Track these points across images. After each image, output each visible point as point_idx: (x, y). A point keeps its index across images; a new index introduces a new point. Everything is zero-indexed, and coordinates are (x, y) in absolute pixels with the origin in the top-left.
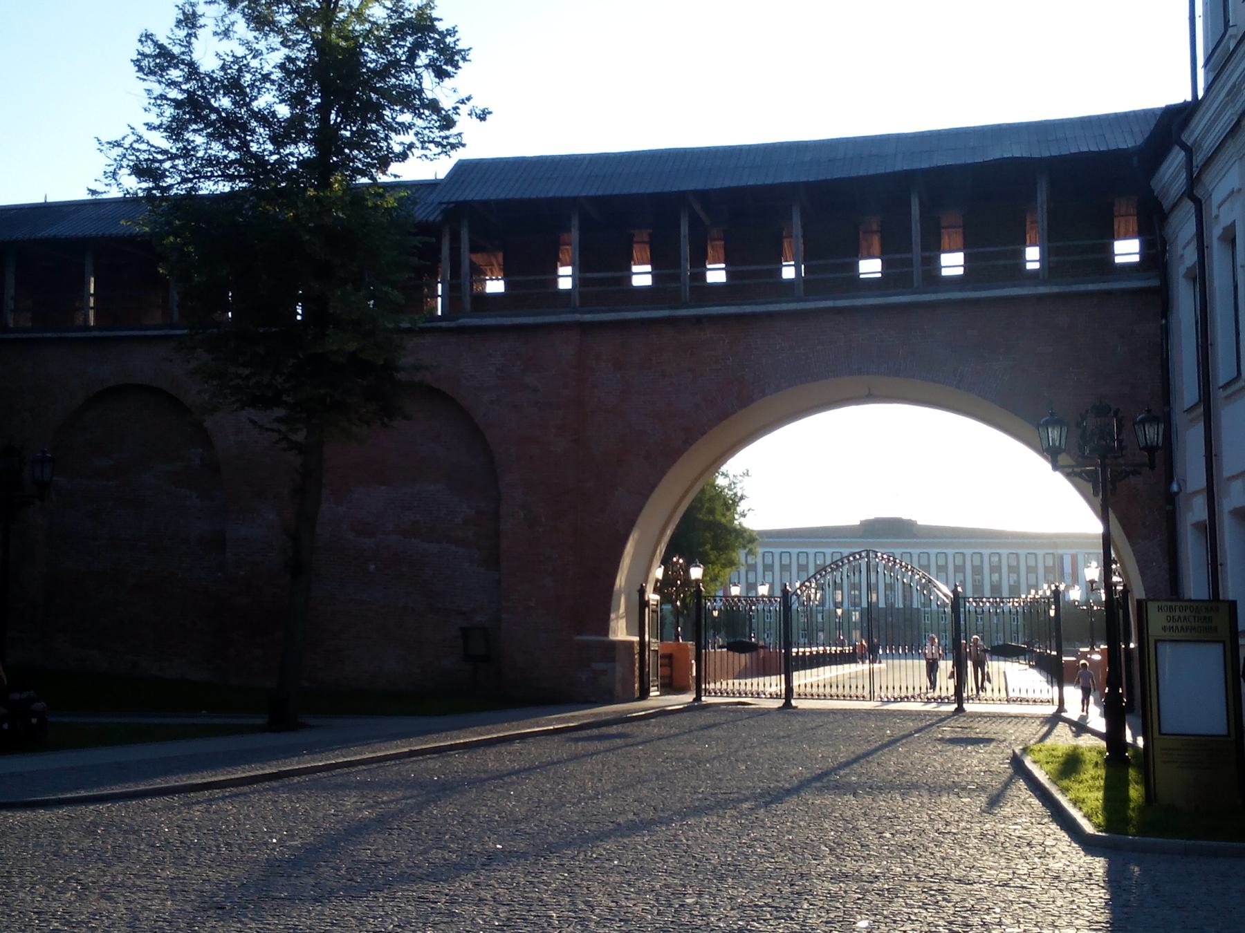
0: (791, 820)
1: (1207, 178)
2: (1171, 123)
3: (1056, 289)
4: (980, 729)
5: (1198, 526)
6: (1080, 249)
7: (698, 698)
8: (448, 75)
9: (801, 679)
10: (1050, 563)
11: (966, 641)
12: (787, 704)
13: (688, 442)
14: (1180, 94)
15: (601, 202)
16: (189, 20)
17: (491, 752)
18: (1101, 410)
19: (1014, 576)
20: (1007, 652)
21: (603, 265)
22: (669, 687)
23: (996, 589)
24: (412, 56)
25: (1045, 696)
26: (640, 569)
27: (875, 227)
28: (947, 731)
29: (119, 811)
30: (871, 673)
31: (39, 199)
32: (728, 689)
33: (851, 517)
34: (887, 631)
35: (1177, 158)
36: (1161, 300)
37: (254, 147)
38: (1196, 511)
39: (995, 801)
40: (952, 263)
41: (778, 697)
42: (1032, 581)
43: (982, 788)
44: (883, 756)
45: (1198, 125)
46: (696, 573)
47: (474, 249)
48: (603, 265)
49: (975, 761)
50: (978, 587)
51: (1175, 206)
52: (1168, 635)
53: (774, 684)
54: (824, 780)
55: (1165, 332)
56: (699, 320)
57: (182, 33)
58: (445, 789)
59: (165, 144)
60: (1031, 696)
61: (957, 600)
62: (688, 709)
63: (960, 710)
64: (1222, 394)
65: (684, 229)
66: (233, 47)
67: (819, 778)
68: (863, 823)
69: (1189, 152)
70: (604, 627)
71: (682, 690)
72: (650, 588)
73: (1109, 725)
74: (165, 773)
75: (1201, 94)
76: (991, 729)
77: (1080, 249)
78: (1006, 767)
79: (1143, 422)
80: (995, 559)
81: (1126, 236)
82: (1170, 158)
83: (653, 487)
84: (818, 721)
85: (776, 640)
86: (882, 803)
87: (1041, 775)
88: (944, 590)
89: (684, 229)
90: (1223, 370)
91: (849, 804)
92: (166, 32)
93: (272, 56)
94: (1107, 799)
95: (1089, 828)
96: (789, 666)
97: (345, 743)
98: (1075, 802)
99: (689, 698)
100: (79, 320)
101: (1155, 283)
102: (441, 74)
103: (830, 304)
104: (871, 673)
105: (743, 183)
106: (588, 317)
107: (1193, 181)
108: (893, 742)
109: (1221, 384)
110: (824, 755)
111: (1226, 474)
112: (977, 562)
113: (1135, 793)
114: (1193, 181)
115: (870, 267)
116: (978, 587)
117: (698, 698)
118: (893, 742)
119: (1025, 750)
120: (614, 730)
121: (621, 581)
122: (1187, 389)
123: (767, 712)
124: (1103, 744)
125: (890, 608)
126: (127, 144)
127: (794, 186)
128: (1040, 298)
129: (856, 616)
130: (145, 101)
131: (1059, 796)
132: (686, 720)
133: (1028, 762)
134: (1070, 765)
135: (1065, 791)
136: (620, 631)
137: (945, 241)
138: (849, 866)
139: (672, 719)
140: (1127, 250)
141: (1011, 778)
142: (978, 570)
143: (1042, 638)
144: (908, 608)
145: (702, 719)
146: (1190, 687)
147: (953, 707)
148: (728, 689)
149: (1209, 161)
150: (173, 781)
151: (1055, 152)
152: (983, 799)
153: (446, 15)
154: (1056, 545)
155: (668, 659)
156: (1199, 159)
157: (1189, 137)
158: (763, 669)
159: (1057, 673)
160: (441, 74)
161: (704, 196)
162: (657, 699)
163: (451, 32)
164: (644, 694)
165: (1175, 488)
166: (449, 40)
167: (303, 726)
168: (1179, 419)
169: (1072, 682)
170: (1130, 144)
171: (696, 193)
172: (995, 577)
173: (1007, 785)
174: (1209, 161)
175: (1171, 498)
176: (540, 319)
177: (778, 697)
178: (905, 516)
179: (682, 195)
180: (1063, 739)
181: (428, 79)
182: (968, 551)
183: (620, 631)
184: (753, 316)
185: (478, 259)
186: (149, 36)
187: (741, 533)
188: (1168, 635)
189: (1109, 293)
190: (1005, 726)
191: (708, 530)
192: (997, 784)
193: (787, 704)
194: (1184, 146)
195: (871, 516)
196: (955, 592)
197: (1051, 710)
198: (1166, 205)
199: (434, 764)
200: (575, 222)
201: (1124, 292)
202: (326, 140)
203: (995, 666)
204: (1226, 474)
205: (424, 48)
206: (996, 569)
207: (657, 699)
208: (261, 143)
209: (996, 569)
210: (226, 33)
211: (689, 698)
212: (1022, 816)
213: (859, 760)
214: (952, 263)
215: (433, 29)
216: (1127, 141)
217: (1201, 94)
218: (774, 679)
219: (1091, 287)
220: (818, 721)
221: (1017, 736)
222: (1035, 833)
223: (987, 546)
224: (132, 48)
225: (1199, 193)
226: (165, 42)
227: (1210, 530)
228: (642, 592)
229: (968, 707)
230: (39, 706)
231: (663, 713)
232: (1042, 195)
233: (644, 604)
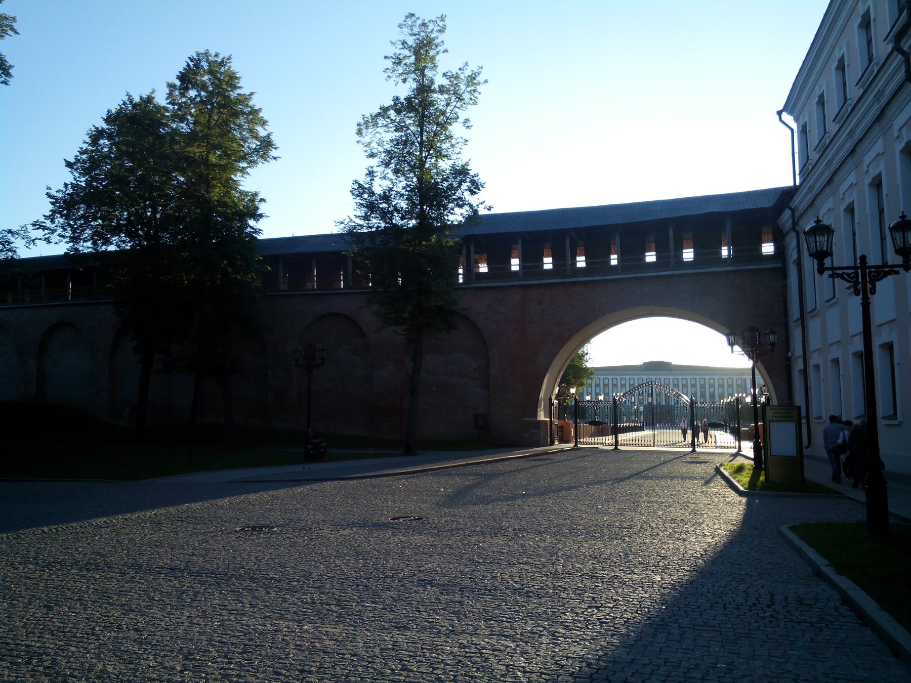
0: (629, 487)
1: (801, 222)
2: (785, 195)
3: (735, 268)
4: (702, 458)
5: (800, 371)
6: (747, 248)
7: (576, 445)
8: (475, 193)
9: (622, 437)
10: (739, 383)
11: (698, 421)
12: (616, 448)
13: (570, 336)
14: (790, 183)
15: (530, 233)
16: (371, 173)
17: (499, 464)
18: (752, 329)
19: (721, 390)
20: (716, 426)
21: (531, 261)
22: (562, 440)
23: (712, 395)
24: (460, 184)
25: (732, 445)
26: (550, 389)
27: (653, 239)
28: (688, 459)
29: (377, 481)
30: (654, 435)
31: (289, 235)
32: (588, 442)
33: (638, 360)
34: (659, 416)
35: (787, 214)
36: (783, 273)
37: (394, 221)
38: (799, 365)
39: (707, 482)
40: (688, 255)
41: (612, 445)
42: (730, 392)
43: (702, 478)
44: (662, 467)
45: (797, 200)
46: (573, 391)
47: (476, 253)
48: (531, 261)
49: (699, 469)
50: (703, 395)
51: (788, 232)
52: (774, 419)
53: (610, 439)
54: (637, 475)
55: (785, 286)
56: (575, 283)
57: (368, 179)
58: (490, 476)
59: (362, 222)
60: (726, 445)
61: (692, 403)
62: (572, 450)
63: (694, 450)
64: (809, 315)
65: (568, 244)
66: (386, 184)
67: (636, 474)
68: (656, 488)
69: (793, 210)
70: (536, 415)
71: (568, 442)
72: (553, 398)
73: (755, 455)
74: (389, 468)
75: (798, 183)
76: (708, 458)
77: (747, 248)
78: (713, 471)
79: (769, 334)
80: (712, 381)
81: (768, 242)
82: (784, 213)
83: (556, 355)
84: (631, 455)
85: (612, 421)
86: (663, 483)
87: (726, 473)
88: (686, 398)
89: (568, 244)
90: (809, 307)
91: (651, 483)
92: (363, 179)
93: (400, 185)
94: (750, 482)
95: (742, 489)
96: (616, 431)
97: (448, 459)
98: (738, 482)
99: (572, 445)
100: (309, 285)
101: (780, 265)
102: (473, 193)
103: (633, 275)
104: (654, 435)
105: (594, 224)
106: (526, 283)
107: (795, 224)
108: (665, 463)
109: (809, 310)
110: (636, 467)
111: (811, 350)
112: (702, 382)
113: (762, 478)
114: (795, 224)
115: (651, 257)
116: (703, 395)
117: (576, 445)
118: (665, 463)
119: (721, 465)
120: (544, 457)
121: (542, 395)
122: (795, 312)
123: (608, 451)
124: (752, 462)
125: (659, 404)
126: (346, 222)
127: (617, 225)
128: (728, 272)
129: (641, 409)
130: (355, 207)
131: (737, 484)
132: (573, 454)
133: (722, 469)
134: (740, 469)
135: (734, 478)
136: (542, 417)
137: (685, 245)
138: (653, 499)
139: (567, 453)
140: (768, 248)
141: (715, 475)
142: (703, 386)
143: (733, 419)
144: (668, 405)
145: (579, 454)
146: (783, 440)
147: (690, 449)
148: (588, 442)
149: (801, 216)
150: (391, 472)
151: (733, 209)
152: (703, 481)
153: (473, 170)
154: (742, 374)
155: (561, 428)
156: (797, 214)
157: (793, 205)
158: (602, 433)
159: (739, 436)
160: (473, 193)
161: (575, 230)
162: (557, 446)
163: (476, 175)
164: (552, 443)
165: (790, 355)
166: (476, 179)
167: (415, 454)
168: (792, 325)
169: (746, 439)
170: (768, 206)
171: (574, 229)
172: (712, 390)
173: (712, 477)
174: (801, 216)
175: (789, 359)
176: (506, 284)
177: (612, 445)
178: (666, 360)
179: (566, 230)
180: (739, 461)
181: (467, 195)
182: (698, 377)
183: (542, 417)
184: (598, 281)
185: (477, 256)
186: (356, 182)
187: (586, 370)
188: (774, 419)
189: (760, 269)
190: (713, 457)
191: (576, 372)
192: (708, 477)
193: (616, 448)
194: (791, 209)
195: (649, 360)
196: (691, 399)
197: (735, 451)
198: (784, 232)
199: (478, 468)
200: (520, 242)
201: (766, 269)
202: (422, 216)
203: (712, 432)
204: (811, 350)
205: (465, 181)
206: (711, 386)
207: (557, 446)
208: (397, 220)
209: (711, 386)
210: (384, 178)
211: (572, 445)
212: (718, 486)
213: (653, 467)
214: (688, 255)
215: (468, 174)
216: (767, 204)
217: (798, 183)
218: (610, 437)
219: (751, 267)
220: (631, 455)
221: (718, 461)
222: (722, 492)
223: (708, 374)
224: (350, 186)
225: (798, 228)
226: (362, 183)
227: (805, 372)
228: (550, 399)
229: (697, 450)
230: (324, 444)
231: (562, 451)
232: (728, 227)
233: (551, 404)
